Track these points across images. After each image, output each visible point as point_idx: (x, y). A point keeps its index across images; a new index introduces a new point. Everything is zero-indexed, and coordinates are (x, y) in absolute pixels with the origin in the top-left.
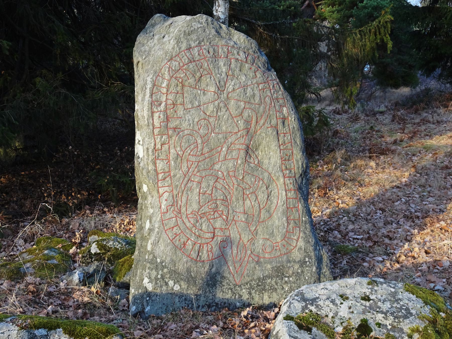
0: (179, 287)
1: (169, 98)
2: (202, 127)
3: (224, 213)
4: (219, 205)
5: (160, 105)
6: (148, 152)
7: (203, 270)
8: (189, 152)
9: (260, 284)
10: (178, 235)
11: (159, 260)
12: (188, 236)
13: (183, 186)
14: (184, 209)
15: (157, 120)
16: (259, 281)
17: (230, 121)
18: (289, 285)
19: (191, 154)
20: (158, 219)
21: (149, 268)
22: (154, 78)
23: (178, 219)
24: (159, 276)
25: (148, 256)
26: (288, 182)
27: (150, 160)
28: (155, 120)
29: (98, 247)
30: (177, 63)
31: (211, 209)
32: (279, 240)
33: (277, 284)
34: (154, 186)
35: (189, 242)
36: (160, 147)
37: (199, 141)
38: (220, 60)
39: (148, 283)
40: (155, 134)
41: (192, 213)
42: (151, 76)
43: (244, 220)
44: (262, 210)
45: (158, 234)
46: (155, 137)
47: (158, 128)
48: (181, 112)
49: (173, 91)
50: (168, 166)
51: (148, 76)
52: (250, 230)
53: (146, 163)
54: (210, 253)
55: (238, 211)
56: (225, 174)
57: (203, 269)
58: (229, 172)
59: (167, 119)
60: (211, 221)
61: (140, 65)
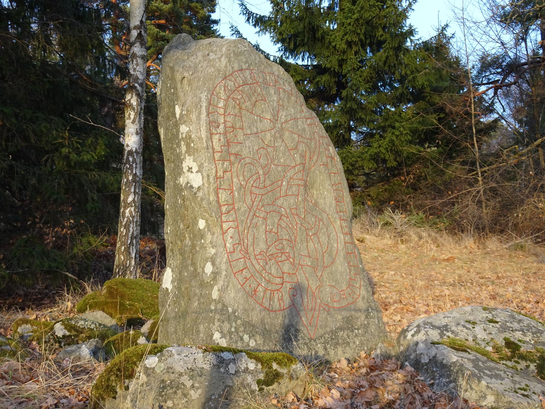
0: (254, 343)
1: (228, 120)
2: (262, 157)
3: (291, 255)
4: (286, 246)
5: (218, 127)
6: (208, 179)
7: (278, 321)
8: (252, 183)
9: (334, 337)
10: (248, 279)
11: (230, 310)
12: (258, 280)
13: (248, 221)
14: (251, 249)
15: (217, 143)
16: (332, 334)
17: (287, 154)
18: (359, 338)
19: (254, 185)
20: (224, 260)
21: (219, 320)
22: (209, 96)
23: (247, 260)
24: (233, 330)
25: (216, 306)
26: (344, 225)
27: (212, 189)
28: (214, 144)
29: (66, 328)
30: (232, 83)
31: (278, 250)
32: (345, 288)
33: (348, 337)
34: (217, 221)
35: (260, 288)
36: (222, 174)
37: (261, 172)
38: (270, 88)
39: (221, 338)
40: (216, 159)
41: (260, 254)
42: (206, 94)
43: (310, 264)
44: (324, 254)
45: (226, 278)
46: (216, 162)
47: (219, 152)
48: (241, 138)
49: (232, 113)
50: (231, 197)
51: (202, 93)
52: (317, 276)
53: (206, 192)
54: (281, 301)
55: (302, 254)
56: (288, 211)
57: (276, 320)
58: (291, 209)
59: (228, 143)
60: (279, 263)
61: (185, 81)
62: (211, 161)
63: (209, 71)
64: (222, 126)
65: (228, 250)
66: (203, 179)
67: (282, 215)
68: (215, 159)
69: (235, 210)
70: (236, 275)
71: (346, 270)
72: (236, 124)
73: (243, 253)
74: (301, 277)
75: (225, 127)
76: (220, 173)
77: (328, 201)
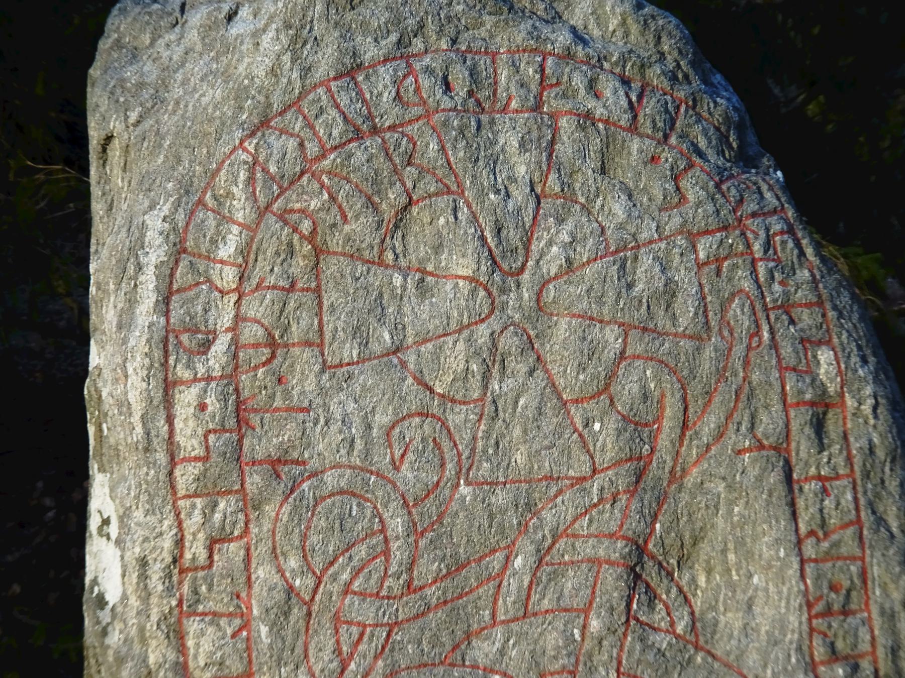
1: (251, 314)
2: (410, 456)
5: (206, 346)
6: (143, 577)
8: (345, 576)
15: (191, 423)
17: (550, 423)
19: (356, 586)
22: (181, 217)
27: (154, 618)
28: (178, 424)
30: (292, 143)
37: (397, 524)
40: (181, 493)
42: (166, 210)
46: (181, 503)
47: (197, 459)
48: (305, 380)
49: (271, 280)
50: (241, 646)
51: (152, 207)
53: (134, 632)
59: (241, 416)
63: (205, 100)
64: (220, 346)
66: (123, 576)
72: (286, 329)
75: (235, 345)
76: (196, 550)
77: (764, 618)
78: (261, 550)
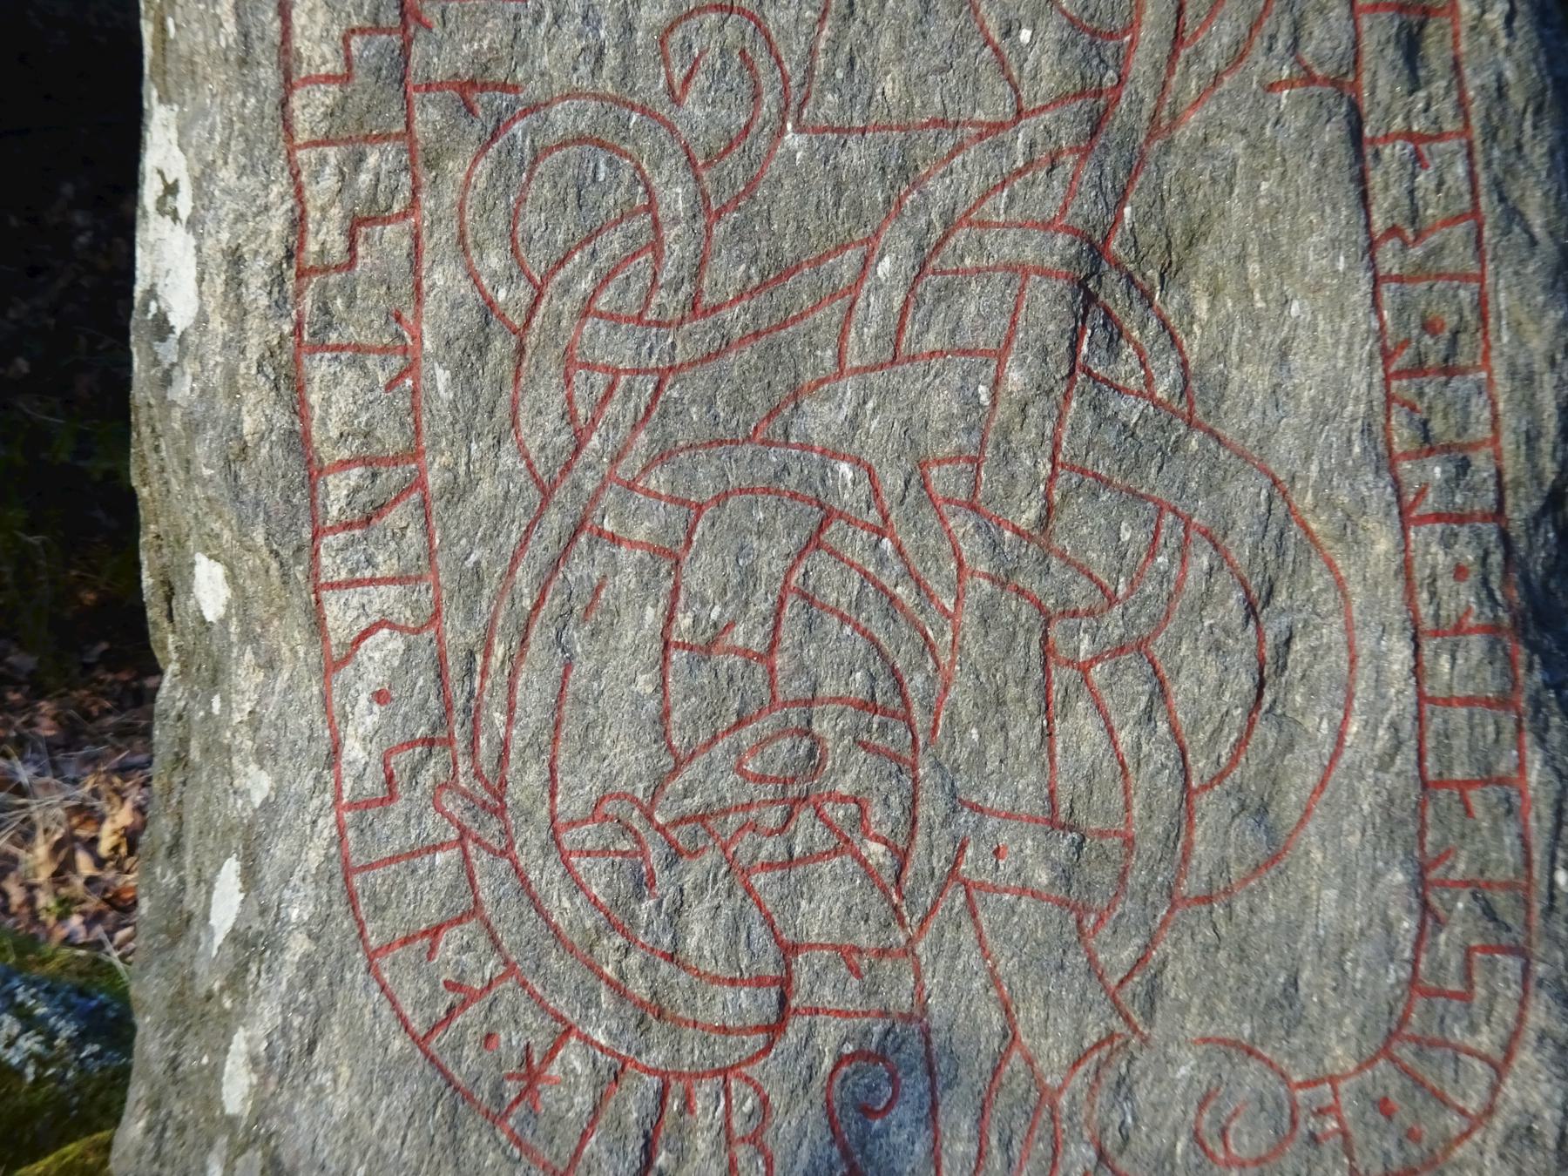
2: (701, 80)
3: (876, 813)
4: (835, 750)
6: (235, 282)
8: (585, 285)
10: (471, 997)
14: (534, 776)
15: (321, 17)
19: (602, 303)
20: (314, 857)
23: (480, 860)
27: (253, 354)
31: (761, 779)
35: (573, 1057)
36: (338, 246)
37: (676, 197)
40: (302, 137)
41: (596, 813)
44: (1203, 801)
45: (310, 980)
47: (329, 78)
50: (403, 403)
52: (1094, 969)
53: (217, 378)
54: (742, 1152)
55: (994, 799)
56: (892, 481)
60: (759, 880)
62: (262, 151)
65: (347, 785)
66: (200, 280)
67: (828, 516)
68: (288, 125)
69: (424, 503)
70: (385, 962)
71: (1389, 927)
73: (452, 805)
74: (952, 986)
76: (326, 236)
77: (1308, 374)
78: (440, 238)
